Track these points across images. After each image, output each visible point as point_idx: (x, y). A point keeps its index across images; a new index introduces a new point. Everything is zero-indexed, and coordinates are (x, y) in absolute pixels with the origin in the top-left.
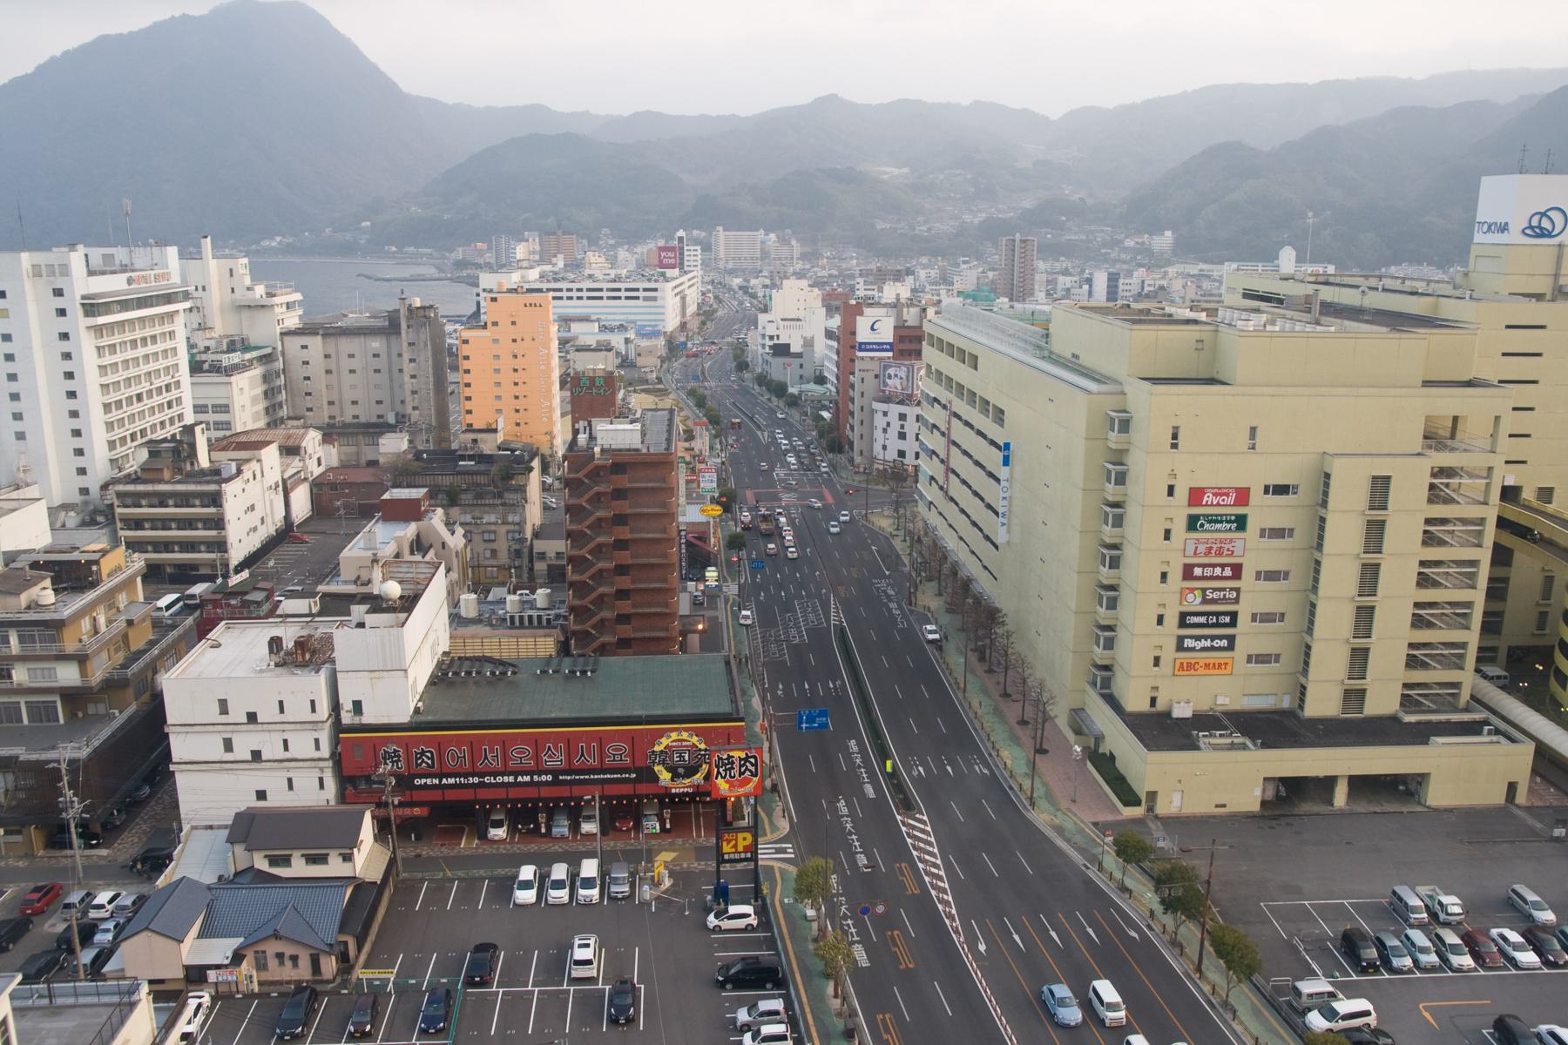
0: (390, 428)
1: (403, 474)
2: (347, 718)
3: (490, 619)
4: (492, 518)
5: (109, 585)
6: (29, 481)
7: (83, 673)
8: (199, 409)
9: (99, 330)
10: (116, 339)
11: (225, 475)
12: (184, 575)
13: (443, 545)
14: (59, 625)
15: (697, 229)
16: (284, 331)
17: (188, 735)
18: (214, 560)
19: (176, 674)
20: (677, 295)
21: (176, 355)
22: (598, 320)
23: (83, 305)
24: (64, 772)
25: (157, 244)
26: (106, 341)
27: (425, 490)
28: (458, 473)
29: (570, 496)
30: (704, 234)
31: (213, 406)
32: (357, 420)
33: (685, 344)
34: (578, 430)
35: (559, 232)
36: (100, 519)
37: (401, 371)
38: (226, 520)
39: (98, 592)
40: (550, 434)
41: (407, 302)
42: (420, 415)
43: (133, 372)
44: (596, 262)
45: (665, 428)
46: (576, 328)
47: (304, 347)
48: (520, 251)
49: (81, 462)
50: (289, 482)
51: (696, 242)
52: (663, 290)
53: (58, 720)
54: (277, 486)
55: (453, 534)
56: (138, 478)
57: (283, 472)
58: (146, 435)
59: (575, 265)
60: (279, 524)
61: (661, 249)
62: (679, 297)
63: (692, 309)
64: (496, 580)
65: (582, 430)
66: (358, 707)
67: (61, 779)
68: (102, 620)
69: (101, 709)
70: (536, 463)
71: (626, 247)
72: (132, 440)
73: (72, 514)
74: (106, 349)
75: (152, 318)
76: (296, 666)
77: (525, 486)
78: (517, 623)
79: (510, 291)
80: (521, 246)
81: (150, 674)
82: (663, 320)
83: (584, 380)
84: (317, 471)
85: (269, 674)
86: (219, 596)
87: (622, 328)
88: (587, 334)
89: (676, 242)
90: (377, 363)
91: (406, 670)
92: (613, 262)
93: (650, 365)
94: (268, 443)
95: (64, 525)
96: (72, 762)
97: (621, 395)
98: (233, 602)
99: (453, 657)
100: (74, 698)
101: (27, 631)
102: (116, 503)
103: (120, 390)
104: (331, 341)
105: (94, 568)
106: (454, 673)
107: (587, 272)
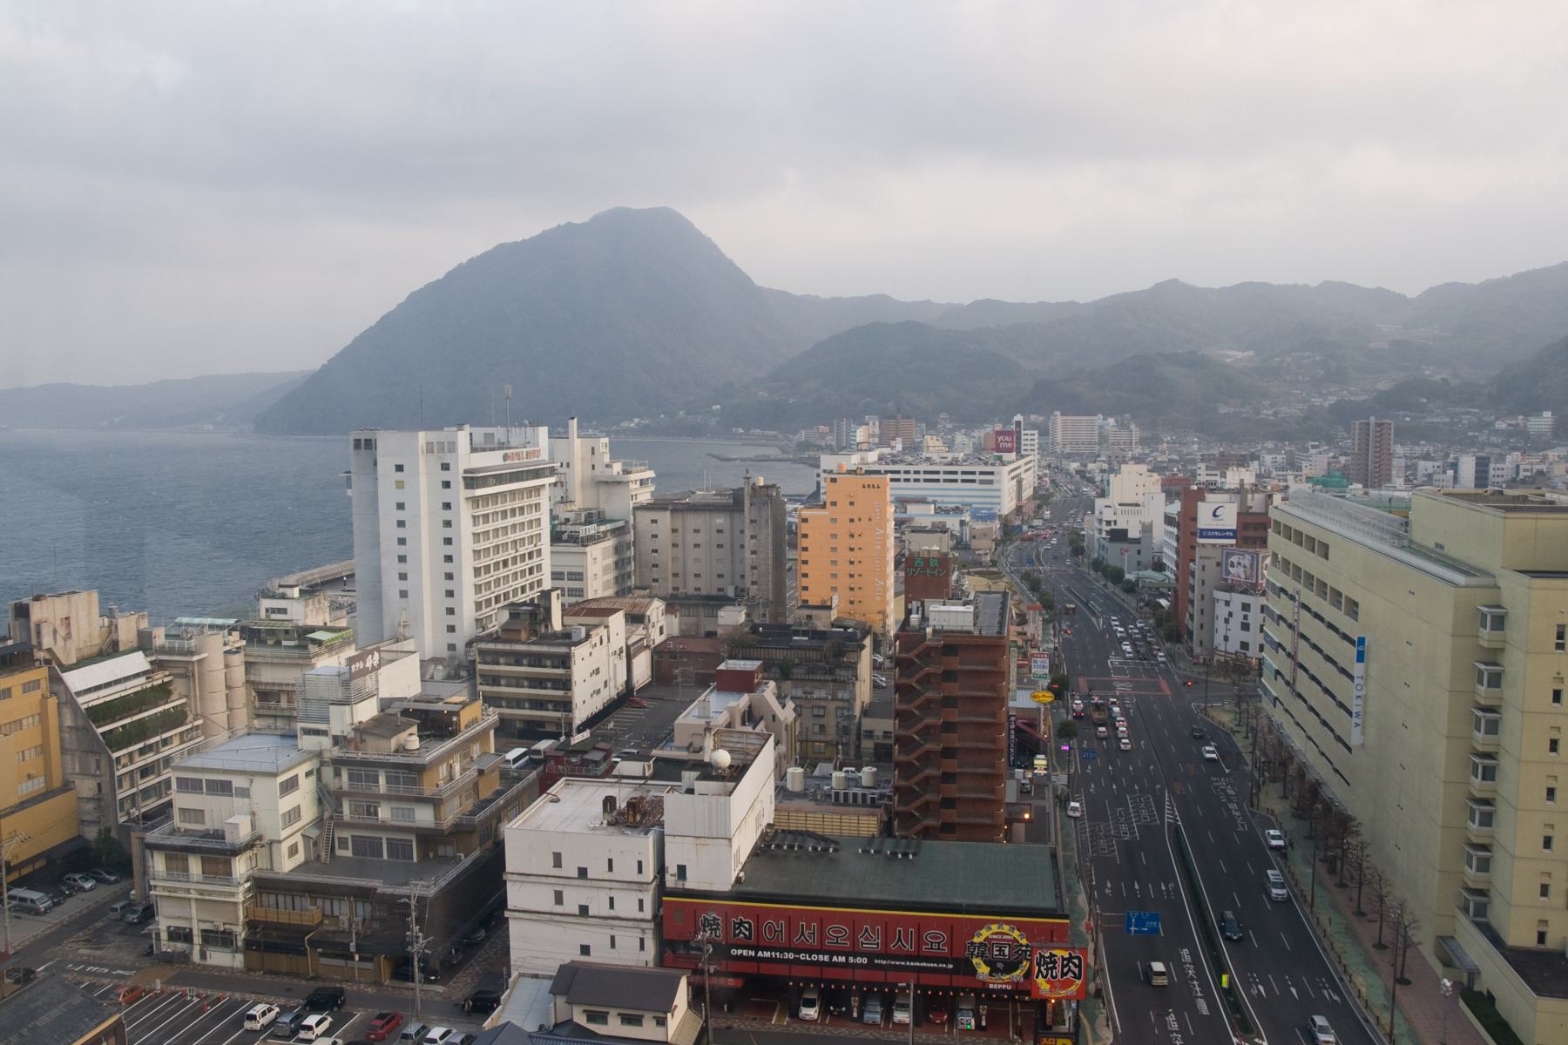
1: (739, 645)
2: (671, 881)
4: (823, 694)
6: (407, 635)
7: (437, 817)
9: (475, 501)
10: (490, 510)
11: (575, 639)
12: (532, 731)
13: (774, 717)
18: (560, 719)
20: (1013, 478)
21: (540, 525)
22: (934, 502)
23: (464, 478)
24: (413, 907)
26: (481, 511)
30: (1041, 418)
31: (568, 573)
33: (1020, 527)
35: (899, 416)
37: (742, 546)
38: (573, 681)
40: (883, 613)
42: (759, 590)
43: (501, 540)
44: (933, 445)
45: (998, 611)
46: (912, 509)
47: (654, 521)
48: (861, 434)
51: (1034, 426)
52: (999, 473)
53: (412, 859)
54: (621, 652)
57: (627, 639)
59: (913, 448)
60: (620, 688)
61: (998, 433)
63: (1028, 492)
65: (914, 610)
66: (682, 870)
68: (457, 768)
69: (450, 851)
70: (868, 642)
71: (963, 431)
72: (496, 603)
73: (440, 667)
74: (481, 519)
75: (521, 491)
76: (627, 826)
77: (856, 663)
78: (860, 801)
79: (853, 472)
81: (495, 821)
82: (999, 504)
83: (918, 561)
84: (659, 639)
86: (561, 753)
87: (957, 510)
88: (923, 515)
89: (1013, 427)
91: (730, 839)
92: (950, 445)
93: (984, 548)
94: (617, 610)
95: (432, 678)
96: (421, 899)
97: (954, 577)
98: (574, 760)
99: (776, 830)
100: (428, 838)
102: (478, 660)
104: (679, 516)
105: (455, 719)
106: (777, 846)
107: (925, 455)
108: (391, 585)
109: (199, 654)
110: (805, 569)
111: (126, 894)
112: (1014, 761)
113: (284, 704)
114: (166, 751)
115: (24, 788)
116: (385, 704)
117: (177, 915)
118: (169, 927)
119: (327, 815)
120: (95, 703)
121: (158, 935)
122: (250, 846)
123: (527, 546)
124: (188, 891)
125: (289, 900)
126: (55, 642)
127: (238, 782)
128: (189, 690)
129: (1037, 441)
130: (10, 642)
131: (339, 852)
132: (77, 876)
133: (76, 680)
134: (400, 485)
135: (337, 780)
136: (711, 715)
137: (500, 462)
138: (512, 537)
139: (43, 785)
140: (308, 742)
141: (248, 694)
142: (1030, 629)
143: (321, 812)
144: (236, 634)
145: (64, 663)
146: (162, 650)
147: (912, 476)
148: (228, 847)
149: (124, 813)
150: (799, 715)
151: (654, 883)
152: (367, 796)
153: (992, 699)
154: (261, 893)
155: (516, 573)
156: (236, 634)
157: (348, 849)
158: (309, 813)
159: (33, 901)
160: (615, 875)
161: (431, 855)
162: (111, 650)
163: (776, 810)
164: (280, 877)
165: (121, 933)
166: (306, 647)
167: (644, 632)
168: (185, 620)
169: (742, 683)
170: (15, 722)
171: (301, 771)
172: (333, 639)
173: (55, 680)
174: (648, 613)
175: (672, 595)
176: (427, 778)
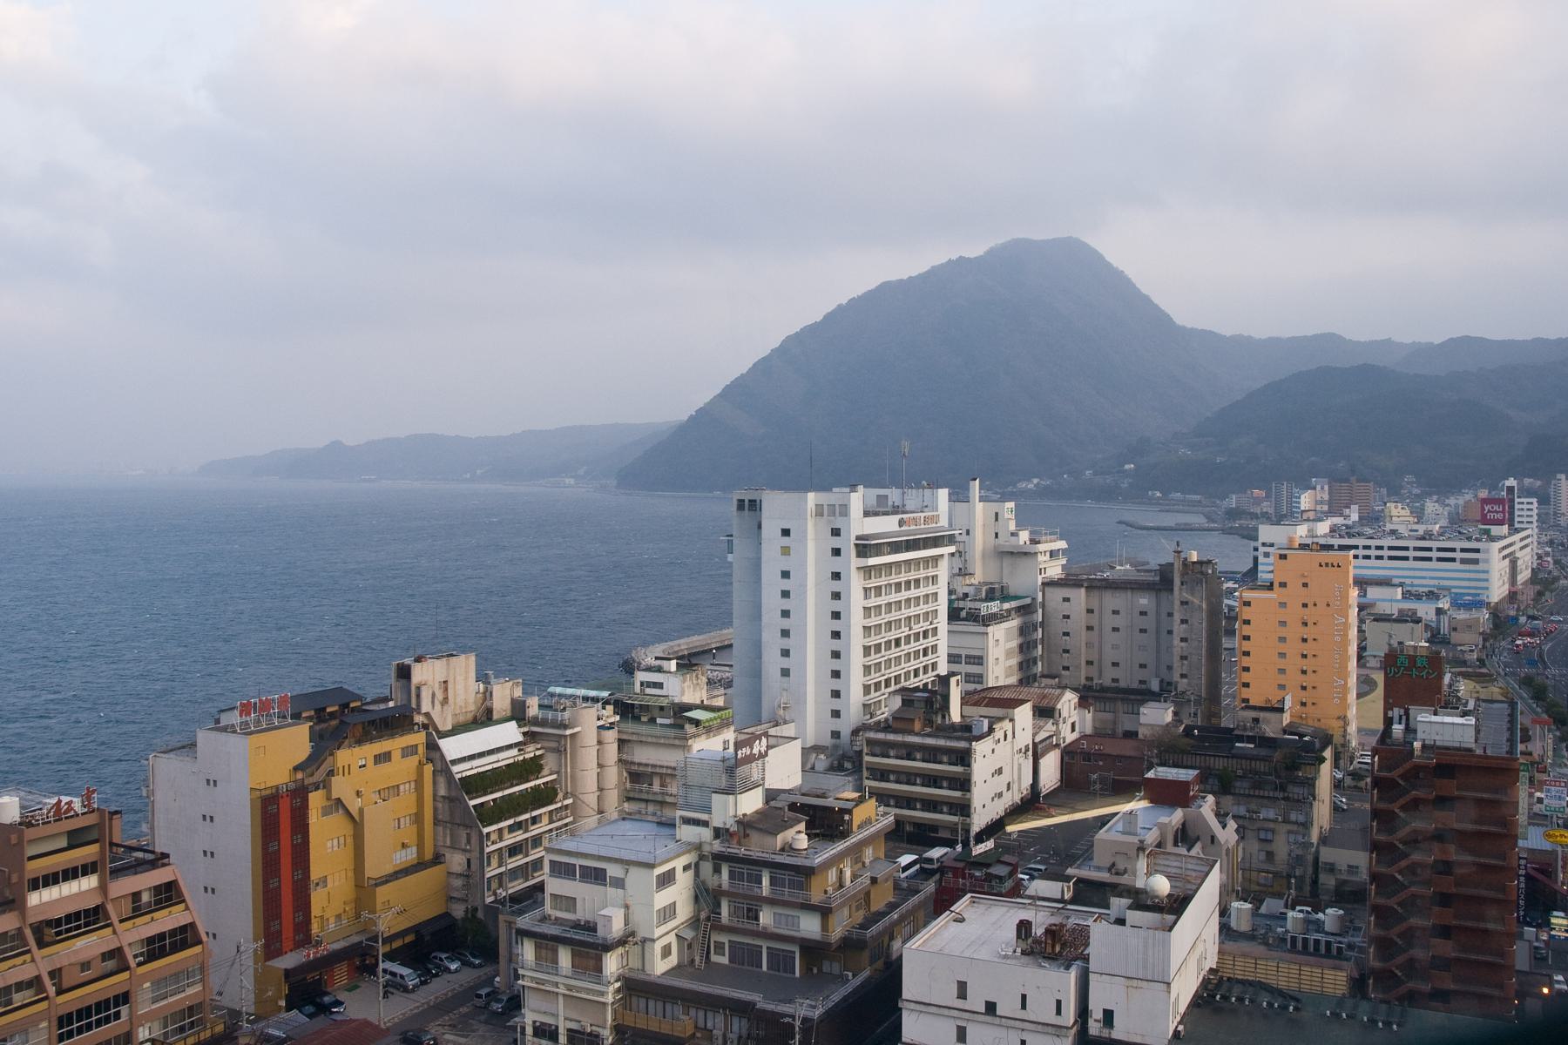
0: (1155, 697)
1: (1169, 751)
2: (1094, 1028)
3: (1265, 936)
4: (1271, 814)
5: (859, 837)
6: (787, 718)
7: (825, 927)
8: (952, 659)
9: (868, 571)
10: (883, 581)
11: (975, 732)
12: (920, 836)
13: (1213, 839)
14: (808, 872)
15: (1530, 477)
16: (1046, 580)
17: (922, 1015)
18: (956, 824)
19: (917, 944)
20: (1504, 557)
21: (936, 600)
22: (1401, 585)
23: (856, 545)
24: (797, 1029)
25: (930, 486)
26: (873, 583)
27: (1196, 772)
28: (1234, 756)
29: (1380, 799)
30: (1539, 483)
31: (967, 657)
32: (1116, 685)
33: (1516, 619)
34: (1392, 718)
35: (1353, 479)
36: (848, 765)
37: (1170, 632)
38: (973, 781)
39: (848, 843)
40: (1344, 719)
41: (1183, 555)
42: (1189, 684)
43: (894, 616)
44: (1398, 514)
45: (1505, 726)
46: (1373, 593)
47: (1066, 600)
48: (1306, 501)
49: (836, 704)
50: (1040, 746)
51: (1528, 493)
52: (1487, 551)
53: (794, 973)
54: (1027, 750)
55: (1224, 827)
56: (889, 727)
57: (1034, 735)
58: (900, 682)
59: (1373, 519)
60: (1025, 792)
61: (1485, 501)
62: (1507, 560)
63: (1524, 576)
64: (1270, 890)
65: (1396, 719)
66: (1108, 1016)
67: (793, 1038)
68: (848, 874)
69: (836, 968)
70: (1328, 753)
71: (1435, 497)
72: (886, 687)
73: (822, 756)
74: (873, 590)
75: (917, 561)
76: (1044, 957)
77: (1314, 779)
78: (1300, 945)
79: (1303, 547)
80: (1306, 494)
81: (886, 939)
82: (1487, 588)
83: (1402, 659)
84: (1070, 737)
85: (1014, 962)
86: (961, 865)
87: (1432, 596)
88: (1388, 600)
89: (1504, 493)
90: (1143, 622)
91: (1169, 984)
92: (1419, 515)
93: (1469, 643)
94: (1022, 702)
95: (813, 768)
96: (805, 1020)
97: (1447, 679)
98: (978, 874)
99: (1222, 977)
100: (813, 951)
101: (781, 874)
102: (865, 751)
103: (880, 633)
104: (1096, 594)
105: (847, 817)
106: (1223, 997)
107: (1389, 527)
108: (772, 662)
109: (573, 728)
110: (1246, 661)
111: (490, 981)
112: (1524, 917)
113: (656, 787)
114: (535, 830)
115: (398, 856)
116: (771, 795)
117: (543, 1009)
118: (534, 1022)
119: (703, 915)
120: (468, 773)
121: (523, 1029)
122: (622, 942)
123: (921, 624)
124: (556, 985)
125: (660, 1005)
126: (433, 707)
127: (613, 871)
128: (560, 766)
129: (1536, 511)
130: (391, 704)
131: (715, 958)
132: (443, 956)
133: (451, 747)
134: (786, 551)
135: (716, 877)
136: (1139, 831)
137: (896, 528)
138: (905, 612)
139: (415, 856)
140: (687, 833)
141: (620, 774)
142: (1536, 747)
143: (698, 911)
144: (610, 708)
145: (441, 729)
146: (535, 721)
147: (1373, 553)
148: (600, 941)
149: (491, 893)
150: (1242, 838)
151: (1075, 1028)
152: (745, 897)
153: (1506, 836)
154: (630, 995)
155: (909, 654)
156: (610, 708)
157: (724, 955)
158: (684, 912)
159: (402, 977)
160: (1029, 1014)
161: (815, 971)
162: (484, 718)
163: (1219, 952)
164: (652, 979)
165: (486, 1022)
166: (682, 727)
167: (1054, 728)
168: (558, 690)
169: (1168, 795)
170: (393, 787)
171: (679, 864)
172: (711, 720)
173: (432, 747)
174: (1059, 706)
175: (1085, 686)
176: (816, 883)
